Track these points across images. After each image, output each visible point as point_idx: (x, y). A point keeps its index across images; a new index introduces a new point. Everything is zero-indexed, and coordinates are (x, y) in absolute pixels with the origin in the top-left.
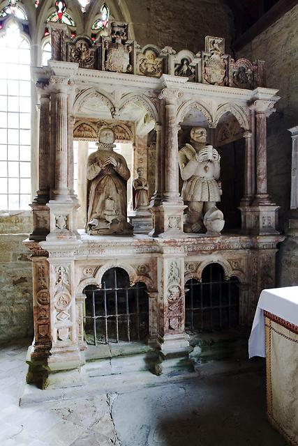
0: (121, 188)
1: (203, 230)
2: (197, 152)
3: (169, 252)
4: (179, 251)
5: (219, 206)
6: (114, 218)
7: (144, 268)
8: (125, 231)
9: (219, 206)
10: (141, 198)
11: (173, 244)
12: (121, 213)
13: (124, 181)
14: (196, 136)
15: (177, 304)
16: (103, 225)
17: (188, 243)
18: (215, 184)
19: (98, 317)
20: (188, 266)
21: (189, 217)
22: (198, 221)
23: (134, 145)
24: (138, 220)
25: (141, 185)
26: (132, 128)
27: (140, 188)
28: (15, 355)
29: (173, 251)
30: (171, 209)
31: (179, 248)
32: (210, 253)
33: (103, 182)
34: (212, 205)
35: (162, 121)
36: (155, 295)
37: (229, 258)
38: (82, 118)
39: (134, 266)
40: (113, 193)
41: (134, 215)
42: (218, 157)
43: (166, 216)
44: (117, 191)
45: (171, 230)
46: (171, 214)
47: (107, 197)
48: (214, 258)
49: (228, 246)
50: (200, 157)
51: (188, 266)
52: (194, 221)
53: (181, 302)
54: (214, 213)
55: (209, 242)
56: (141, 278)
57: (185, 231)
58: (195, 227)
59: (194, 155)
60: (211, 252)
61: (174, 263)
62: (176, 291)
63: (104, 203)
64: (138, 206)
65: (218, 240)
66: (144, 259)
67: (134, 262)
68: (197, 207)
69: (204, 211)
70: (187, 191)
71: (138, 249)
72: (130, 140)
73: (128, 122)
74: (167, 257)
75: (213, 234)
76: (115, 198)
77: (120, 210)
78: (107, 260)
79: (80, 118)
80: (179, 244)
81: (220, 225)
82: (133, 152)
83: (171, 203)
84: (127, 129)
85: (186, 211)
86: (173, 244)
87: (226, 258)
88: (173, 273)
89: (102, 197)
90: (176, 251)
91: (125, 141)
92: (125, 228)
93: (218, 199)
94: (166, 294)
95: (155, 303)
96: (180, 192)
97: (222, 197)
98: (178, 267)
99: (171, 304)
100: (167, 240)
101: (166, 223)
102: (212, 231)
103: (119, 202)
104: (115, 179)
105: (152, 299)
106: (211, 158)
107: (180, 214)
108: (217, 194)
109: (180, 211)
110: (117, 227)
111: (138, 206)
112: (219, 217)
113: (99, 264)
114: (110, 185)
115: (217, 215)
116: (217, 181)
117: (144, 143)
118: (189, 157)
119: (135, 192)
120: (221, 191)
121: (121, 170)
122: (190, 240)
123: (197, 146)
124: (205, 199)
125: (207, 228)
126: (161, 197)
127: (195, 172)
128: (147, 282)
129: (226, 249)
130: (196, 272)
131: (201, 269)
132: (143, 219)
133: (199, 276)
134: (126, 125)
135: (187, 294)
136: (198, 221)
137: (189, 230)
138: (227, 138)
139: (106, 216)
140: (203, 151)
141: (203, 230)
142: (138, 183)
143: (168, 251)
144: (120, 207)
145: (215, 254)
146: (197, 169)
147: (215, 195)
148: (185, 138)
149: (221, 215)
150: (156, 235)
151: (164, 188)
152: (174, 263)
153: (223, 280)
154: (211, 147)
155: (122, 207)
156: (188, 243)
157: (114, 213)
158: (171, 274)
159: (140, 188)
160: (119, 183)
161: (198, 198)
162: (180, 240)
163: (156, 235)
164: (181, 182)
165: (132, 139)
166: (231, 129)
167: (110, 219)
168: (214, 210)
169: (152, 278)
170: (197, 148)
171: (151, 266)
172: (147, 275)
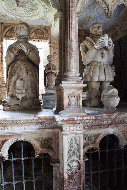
0: (31, 70)
1: (100, 105)
2: (95, 41)
3: (68, 129)
4: (78, 128)
5: (114, 84)
6: (23, 96)
7: (47, 140)
8: (34, 107)
9: (114, 84)
10: (51, 79)
11: (71, 122)
12: (30, 92)
13: (36, 66)
14: (94, 30)
15: (77, 176)
16: (14, 102)
17: (87, 121)
18: (110, 67)
19: (7, 183)
20: (87, 138)
21: (89, 94)
22: (96, 97)
23: (50, 43)
24: (47, 96)
25: (50, 69)
26: (49, 32)
27: (49, 71)
28: (69, 108)
29: (72, 128)
30: (71, 88)
31: (78, 126)
32: (107, 127)
33: (16, 66)
34: (107, 85)
35: (63, 8)
36: (57, 165)
37: (124, 130)
38: (12, 24)
39: (37, 140)
40: (24, 75)
41: (45, 93)
42: (113, 46)
43: (65, 94)
44: (27, 73)
45: (71, 108)
46: (70, 92)
47: (18, 78)
48: (111, 131)
49: (123, 120)
50: (98, 45)
51: (87, 138)
52: (93, 97)
53: (80, 174)
54: (111, 91)
55: (106, 117)
56: (44, 150)
57: (84, 105)
58: (94, 102)
59: (92, 44)
60: (108, 126)
61: (73, 139)
62: (75, 164)
63: (15, 83)
64: (48, 85)
65: (115, 115)
66: (47, 132)
67: (37, 136)
68: (95, 86)
69: (101, 90)
70: (87, 74)
71: (41, 126)
72: (47, 39)
73: (45, 26)
74: (66, 134)
75: (110, 112)
76: (25, 80)
77: (30, 89)
78: (11, 136)
79: (10, 24)
80: (78, 122)
81: (117, 101)
82: (49, 48)
83: (70, 82)
84: (45, 32)
85: (85, 89)
86: (72, 122)
87: (121, 130)
88: (73, 149)
89: (14, 79)
90: (75, 128)
91: (43, 40)
92: (33, 104)
93: (112, 80)
94: (66, 167)
95: (57, 172)
96: (81, 76)
97: (115, 78)
98: (77, 142)
99: (70, 177)
100: (65, 119)
101: (66, 102)
102: (108, 107)
103: (29, 83)
104: (27, 64)
105: (55, 168)
106: (106, 45)
107: (80, 92)
108: (111, 76)
109: (79, 90)
110: (26, 104)
111: (48, 85)
112: (115, 95)
113: (4, 139)
114: (22, 69)
115: (113, 92)
116: (112, 66)
117: (57, 42)
118: (89, 46)
119: (46, 75)
120: (115, 73)
121: (31, 55)
122: (89, 118)
123: (95, 37)
124: (102, 79)
125: (104, 103)
126: (62, 76)
127: (93, 59)
128: (51, 153)
129: (121, 123)
130: (94, 142)
131: (99, 140)
132: (52, 96)
133: (97, 146)
134: (44, 29)
135: (86, 163)
136: (96, 97)
137: (88, 105)
138: (117, 36)
139: (17, 94)
140: (100, 40)
141: (100, 105)
142: (48, 67)
143: (67, 128)
144: (29, 86)
145: (111, 128)
146: (95, 56)
147: (109, 76)
148: (83, 34)
149: (116, 93)
150: (56, 112)
151: (65, 70)
152: (73, 139)
153: (117, 147)
154: (107, 36)
155: (32, 87)
156: (87, 121)
157: (24, 91)
158: (71, 150)
159: (49, 71)
160: (30, 66)
161: (96, 79)
162: (79, 118)
163: (56, 112)
164: (81, 66)
165: (49, 39)
166: (120, 27)
167: (20, 97)
168: (109, 89)
169: (54, 149)
170: (95, 40)
171: (54, 139)
172: (50, 147)
